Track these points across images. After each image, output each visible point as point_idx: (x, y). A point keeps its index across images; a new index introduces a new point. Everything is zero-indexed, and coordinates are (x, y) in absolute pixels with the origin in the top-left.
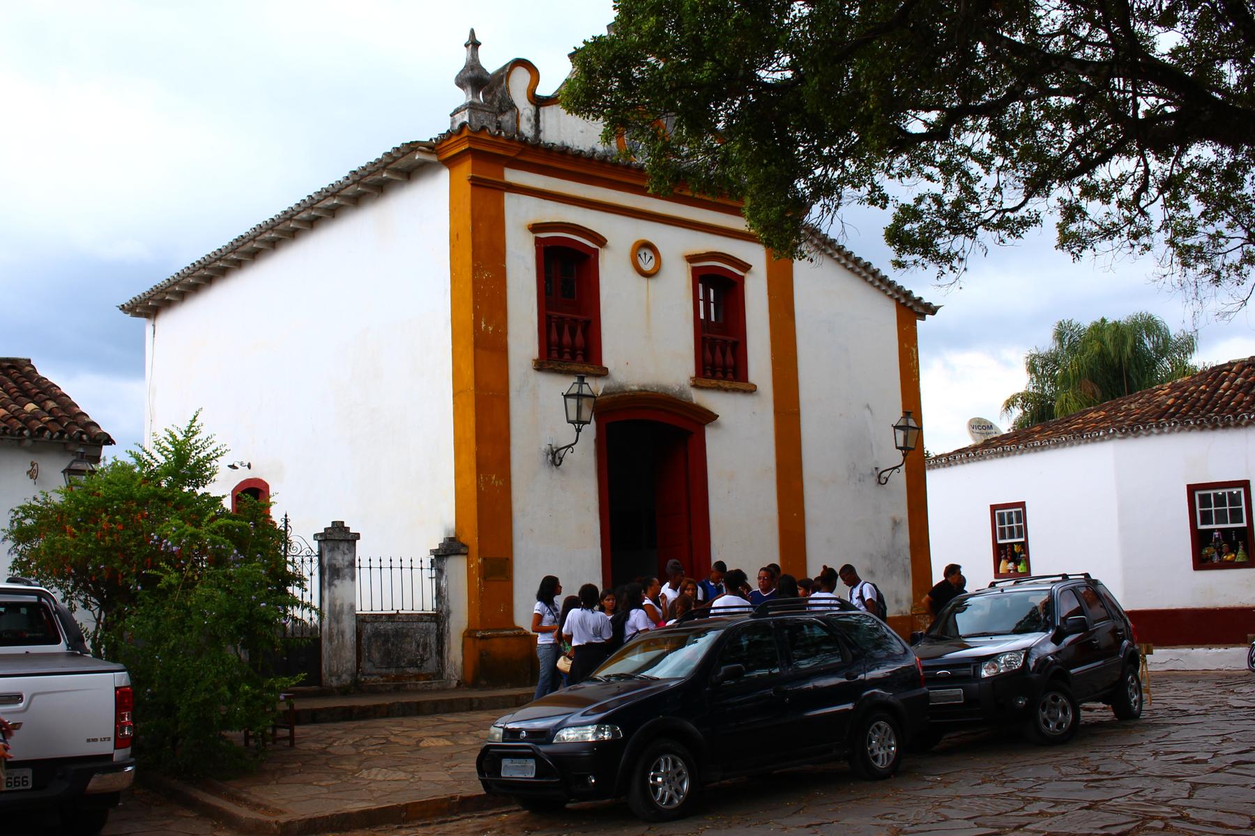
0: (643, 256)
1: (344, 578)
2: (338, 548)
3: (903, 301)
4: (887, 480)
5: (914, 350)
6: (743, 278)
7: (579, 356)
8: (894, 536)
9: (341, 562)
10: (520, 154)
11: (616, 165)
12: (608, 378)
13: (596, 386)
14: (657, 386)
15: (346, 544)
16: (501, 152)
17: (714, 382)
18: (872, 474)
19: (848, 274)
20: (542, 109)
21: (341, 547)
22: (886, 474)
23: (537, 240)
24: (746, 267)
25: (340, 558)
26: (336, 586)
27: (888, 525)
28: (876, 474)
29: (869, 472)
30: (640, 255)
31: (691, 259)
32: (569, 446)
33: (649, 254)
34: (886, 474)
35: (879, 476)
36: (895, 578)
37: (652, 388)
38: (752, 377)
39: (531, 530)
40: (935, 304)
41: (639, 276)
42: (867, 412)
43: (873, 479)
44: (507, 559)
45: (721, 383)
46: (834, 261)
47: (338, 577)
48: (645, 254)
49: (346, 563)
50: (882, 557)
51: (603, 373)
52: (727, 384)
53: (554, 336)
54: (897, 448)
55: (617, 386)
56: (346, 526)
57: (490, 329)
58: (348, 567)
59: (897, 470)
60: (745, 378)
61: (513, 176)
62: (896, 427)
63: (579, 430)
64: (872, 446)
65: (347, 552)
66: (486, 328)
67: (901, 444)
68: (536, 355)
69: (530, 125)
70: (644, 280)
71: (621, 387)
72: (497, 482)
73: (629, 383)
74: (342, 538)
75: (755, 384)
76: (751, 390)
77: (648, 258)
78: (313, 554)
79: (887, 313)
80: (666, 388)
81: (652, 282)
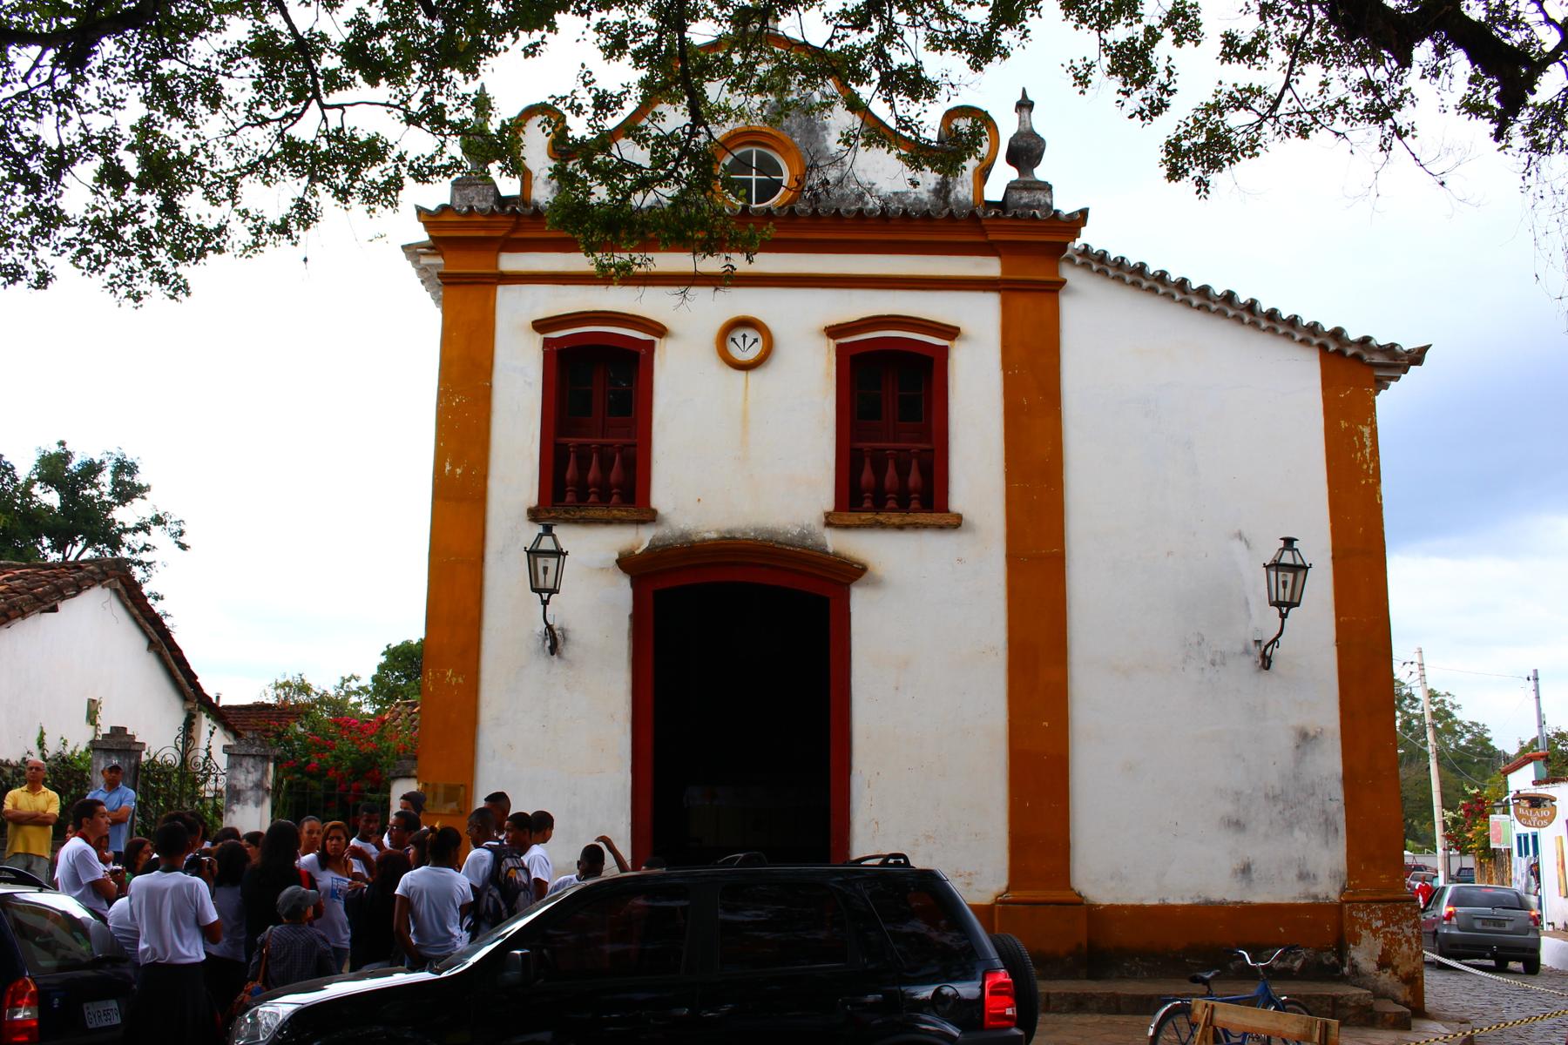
0: (740, 340)
1: (245, 802)
2: (241, 765)
3: (1332, 347)
5: (1366, 431)
6: (946, 348)
7: (914, 501)
8: (1299, 761)
9: (243, 782)
10: (514, 230)
11: (926, 217)
12: (661, 524)
13: (639, 538)
14: (755, 530)
15: (252, 760)
16: (482, 234)
18: (1247, 652)
19: (1198, 316)
21: (245, 764)
25: (243, 777)
26: (234, 812)
27: (1287, 741)
28: (1257, 651)
29: (1240, 648)
30: (733, 340)
31: (833, 332)
32: (1273, 641)
33: (751, 334)
36: (1297, 833)
37: (745, 533)
38: (959, 498)
39: (511, 746)
40: (1407, 343)
41: (726, 366)
42: (1238, 546)
43: (1252, 661)
46: (1163, 298)
47: (238, 801)
48: (744, 336)
49: (250, 785)
50: (1266, 796)
51: (648, 516)
53: (867, 476)
55: (678, 533)
56: (129, 733)
57: (459, 471)
58: (252, 789)
60: (944, 508)
61: (510, 262)
63: (1283, 616)
64: (1247, 603)
65: (252, 770)
66: (452, 471)
68: (533, 500)
69: (549, 189)
70: (741, 375)
71: (684, 535)
72: (454, 679)
73: (701, 529)
74: (243, 752)
76: (955, 523)
77: (749, 341)
78: (219, 772)
80: (773, 532)
81: (754, 376)
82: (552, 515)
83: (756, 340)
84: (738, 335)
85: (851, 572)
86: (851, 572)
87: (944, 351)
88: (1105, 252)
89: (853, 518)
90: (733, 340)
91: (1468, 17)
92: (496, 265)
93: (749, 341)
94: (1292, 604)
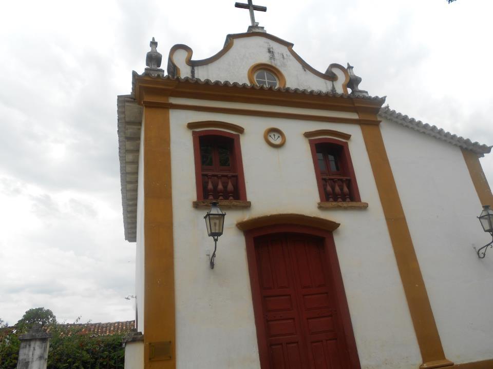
4: (484, 255)
6: (347, 143)
13: (246, 216)
17: (334, 203)
20: (196, 68)
22: (483, 251)
23: (194, 133)
24: (348, 137)
30: (270, 136)
33: (277, 135)
34: (483, 251)
35: (478, 254)
38: (364, 197)
44: (170, 342)
45: (340, 204)
51: (247, 206)
52: (345, 204)
54: (486, 231)
59: (490, 246)
62: (480, 218)
63: (216, 240)
67: (487, 228)
68: (195, 198)
75: (367, 202)
76: (364, 207)
79: (458, 161)
82: (205, 204)
83: (279, 137)
84: (272, 134)
85: (334, 226)
86: (334, 226)
87: (347, 143)
88: (400, 113)
89: (329, 204)
90: (270, 136)
91: (207, 82)
92: (168, 101)
93: (276, 137)
94: (220, 234)
